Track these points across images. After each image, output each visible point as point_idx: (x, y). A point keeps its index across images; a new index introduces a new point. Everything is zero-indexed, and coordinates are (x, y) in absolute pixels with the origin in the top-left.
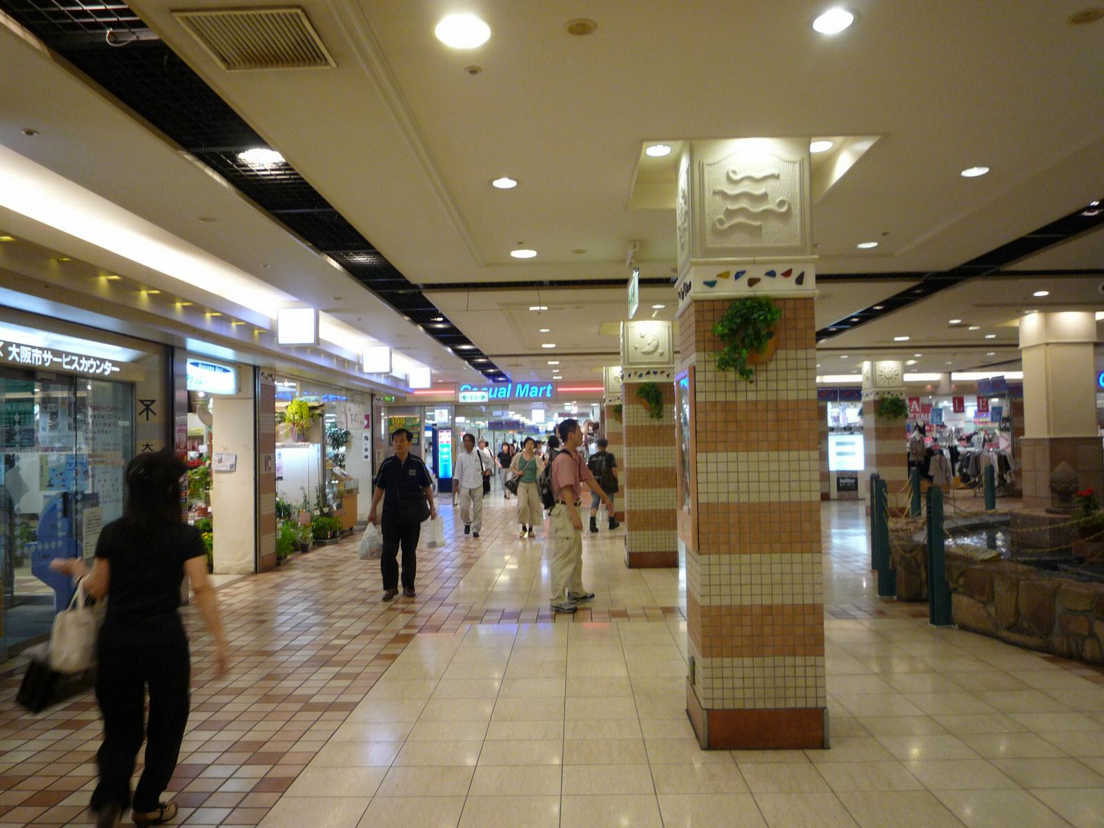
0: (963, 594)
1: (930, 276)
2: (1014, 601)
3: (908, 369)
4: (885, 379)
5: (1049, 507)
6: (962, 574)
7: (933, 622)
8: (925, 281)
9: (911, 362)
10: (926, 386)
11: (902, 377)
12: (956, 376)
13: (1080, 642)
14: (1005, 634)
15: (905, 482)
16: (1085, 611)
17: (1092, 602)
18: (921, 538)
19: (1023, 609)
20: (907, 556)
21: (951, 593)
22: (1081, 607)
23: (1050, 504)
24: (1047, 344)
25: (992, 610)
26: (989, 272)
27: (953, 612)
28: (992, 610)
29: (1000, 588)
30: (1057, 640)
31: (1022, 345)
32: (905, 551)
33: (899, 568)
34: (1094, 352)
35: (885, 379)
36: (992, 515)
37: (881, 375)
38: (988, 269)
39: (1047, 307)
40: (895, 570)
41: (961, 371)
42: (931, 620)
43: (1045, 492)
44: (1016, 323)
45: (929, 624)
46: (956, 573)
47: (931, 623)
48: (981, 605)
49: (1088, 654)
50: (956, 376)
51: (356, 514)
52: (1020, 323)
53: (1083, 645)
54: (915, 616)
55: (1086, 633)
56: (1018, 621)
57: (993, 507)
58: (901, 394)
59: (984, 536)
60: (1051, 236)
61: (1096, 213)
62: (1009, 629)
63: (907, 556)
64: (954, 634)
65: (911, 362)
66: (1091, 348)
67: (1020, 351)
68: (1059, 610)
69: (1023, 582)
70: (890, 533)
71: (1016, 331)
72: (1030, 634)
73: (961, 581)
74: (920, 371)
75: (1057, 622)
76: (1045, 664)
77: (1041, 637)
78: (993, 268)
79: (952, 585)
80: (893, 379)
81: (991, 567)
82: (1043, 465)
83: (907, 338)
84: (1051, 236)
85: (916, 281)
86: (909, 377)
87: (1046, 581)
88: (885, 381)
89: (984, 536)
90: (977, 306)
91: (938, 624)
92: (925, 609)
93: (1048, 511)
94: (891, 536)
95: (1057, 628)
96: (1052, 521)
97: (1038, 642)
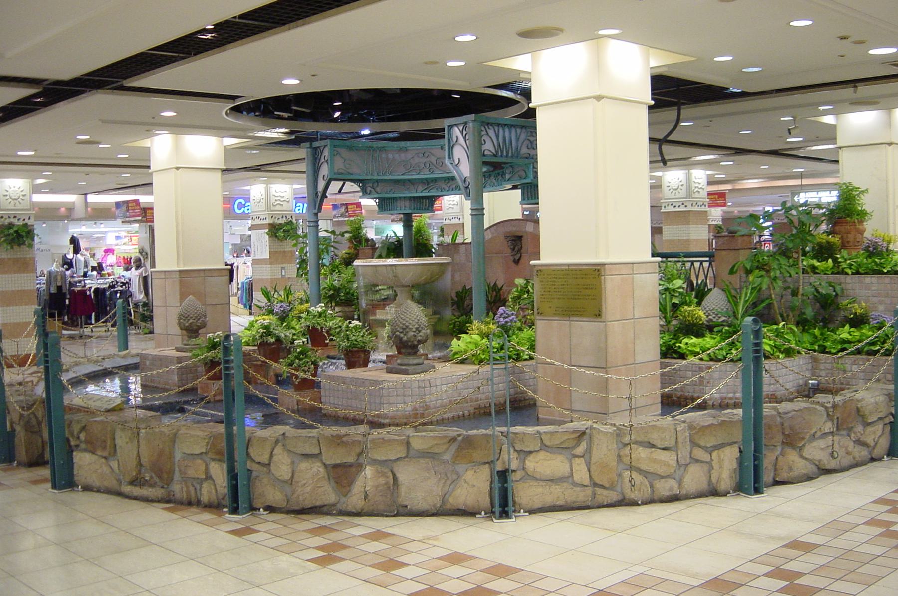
0: (86, 450)
1: (50, 84)
2: (135, 453)
3: (37, 189)
4: (10, 200)
5: (180, 345)
6: (84, 429)
7: (54, 487)
8: (44, 88)
9: (40, 181)
10: (60, 209)
11: (31, 197)
12: (92, 198)
13: (198, 487)
14: (127, 489)
15: (30, 323)
16: (201, 453)
17: (207, 445)
18: (40, 390)
19: (144, 461)
20: (26, 413)
21: (72, 451)
22: (197, 451)
23: (180, 341)
24: (177, 168)
25: (114, 465)
26: (112, 86)
27: (75, 473)
28: (114, 465)
29: (122, 440)
30: (178, 489)
31: (152, 168)
32: (23, 408)
33: (18, 428)
34: (222, 178)
35: (10, 200)
36: (124, 357)
37: (6, 195)
38: (113, 83)
39: (177, 127)
40: (14, 430)
41: (99, 192)
42: (52, 486)
43: (175, 330)
44: (146, 143)
45: (50, 490)
46: (76, 428)
47: (53, 488)
48: (103, 460)
49: (205, 499)
50: (92, 198)
51: (5, 178)
52: (151, 143)
53: (200, 490)
54: (36, 482)
55: (204, 477)
56: (140, 474)
57: (126, 347)
58: (29, 219)
59: (117, 381)
60: (16, 106)
61: (209, 36)
62: (132, 483)
63: (26, 413)
64: (78, 497)
65: (40, 181)
66: (219, 174)
67: (151, 174)
68: (178, 456)
69: (143, 431)
70: (7, 388)
71: (148, 150)
72: (153, 485)
73: (82, 436)
74: (53, 191)
75: (177, 469)
76: (167, 515)
77: (162, 487)
78: (117, 82)
79: (73, 443)
80: (21, 197)
81: (112, 418)
82: (174, 299)
83: (88, 137)
84: (16, 106)
85: (38, 89)
86: (38, 198)
87: (169, 422)
88: (7, 199)
89: (117, 381)
90: (104, 121)
91: (60, 489)
92: (46, 472)
93: (178, 349)
94: (8, 391)
95: (177, 476)
96: (179, 360)
97: (157, 492)
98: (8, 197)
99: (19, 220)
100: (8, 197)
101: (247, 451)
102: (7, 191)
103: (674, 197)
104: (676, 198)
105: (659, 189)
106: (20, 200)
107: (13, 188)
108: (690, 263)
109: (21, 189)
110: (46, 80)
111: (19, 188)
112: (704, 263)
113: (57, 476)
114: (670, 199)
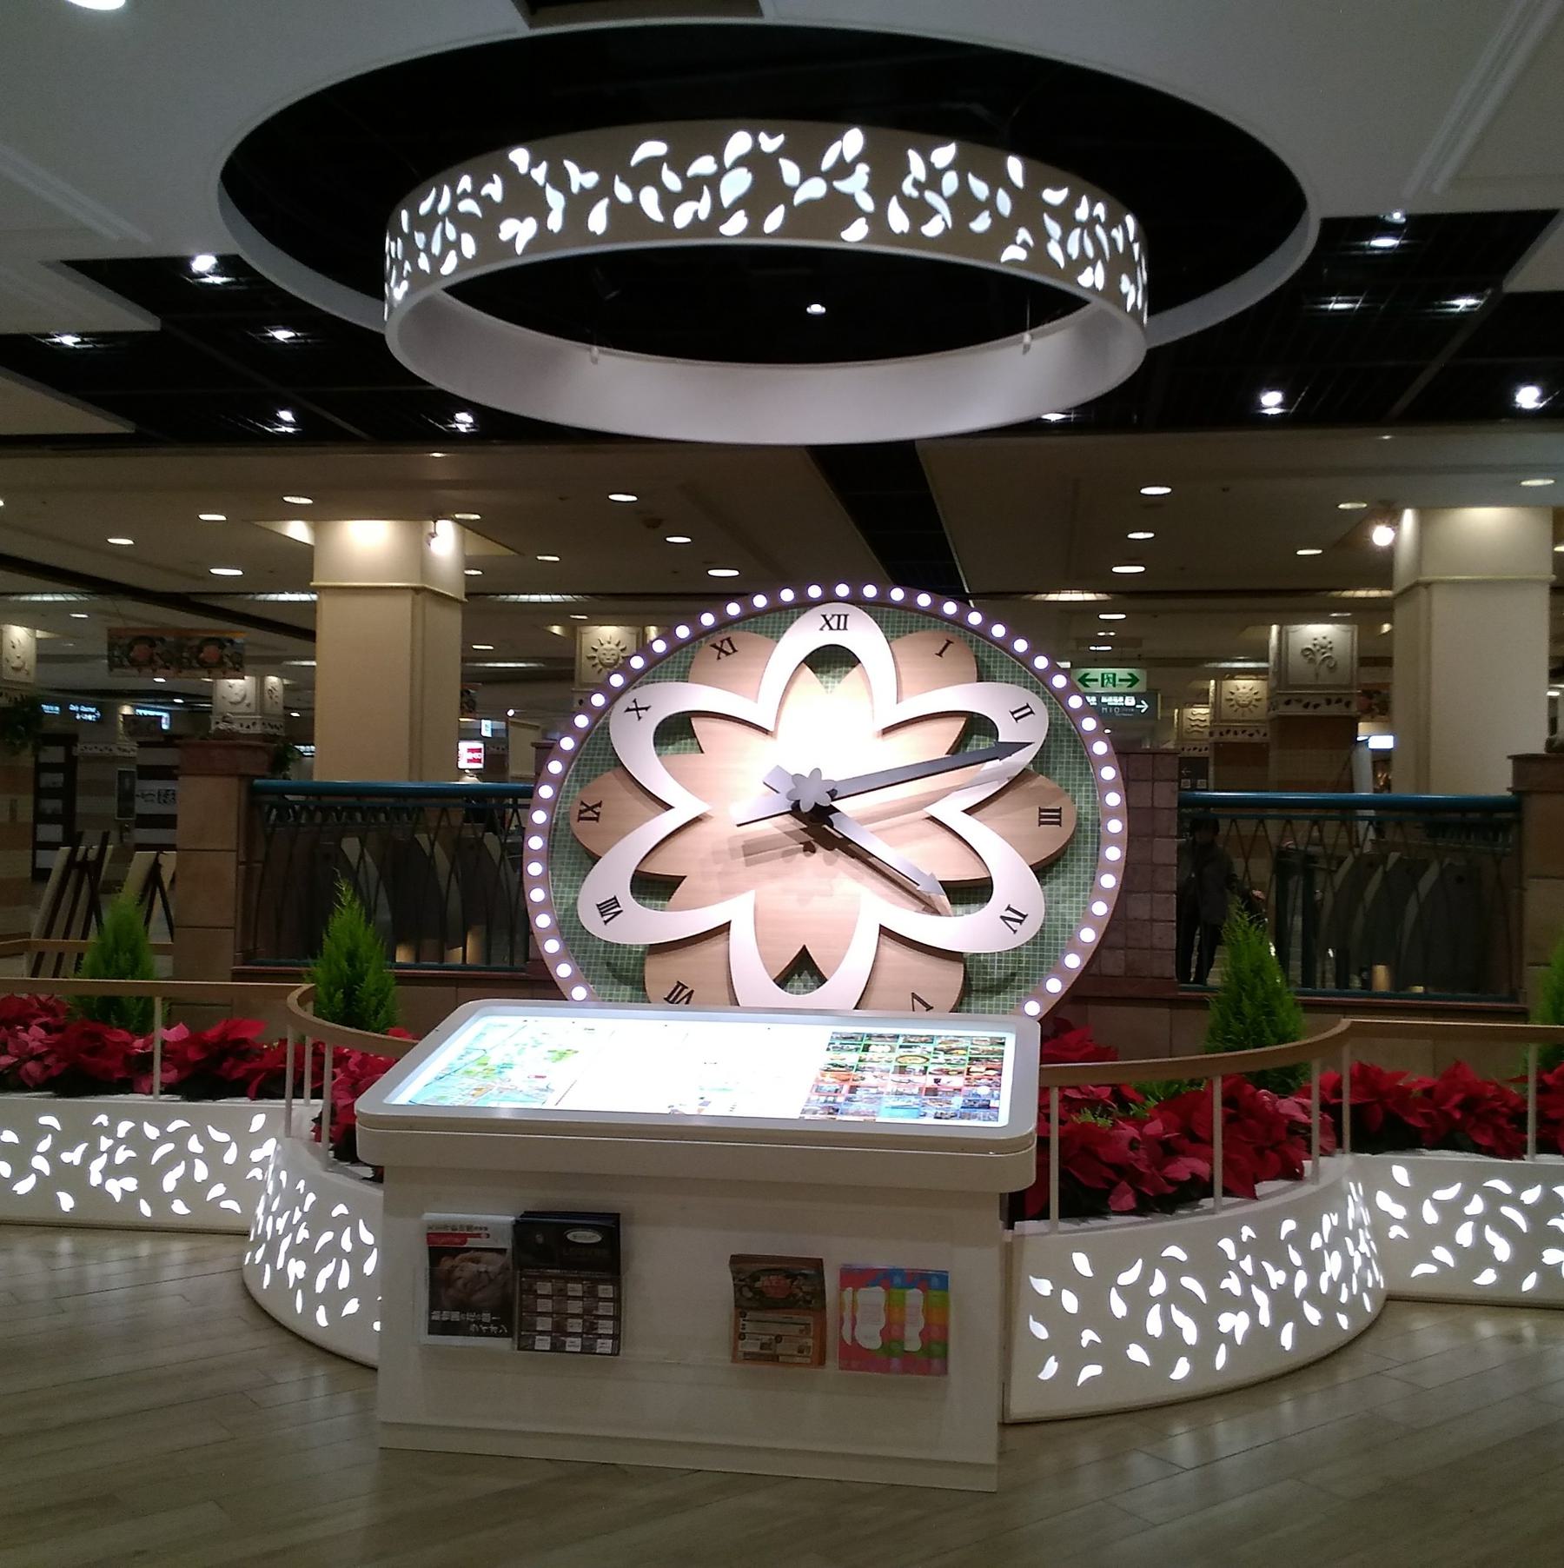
4: (1236, 707)
35: (1236, 707)
37: (1231, 700)
80: (1254, 703)
88: (1232, 706)
98: (597, 661)
99: (1236, 733)
100: (597, 661)
101: (840, 1333)
102: (1233, 693)
103: (1241, 718)
104: (1243, 721)
105: (44, 652)
106: (1251, 707)
107: (1242, 690)
108: (1254, 822)
109: (621, 647)
110: (429, 384)
111: (617, 645)
112: (1241, 823)
113: (1085, 1234)
114: (1232, 721)
